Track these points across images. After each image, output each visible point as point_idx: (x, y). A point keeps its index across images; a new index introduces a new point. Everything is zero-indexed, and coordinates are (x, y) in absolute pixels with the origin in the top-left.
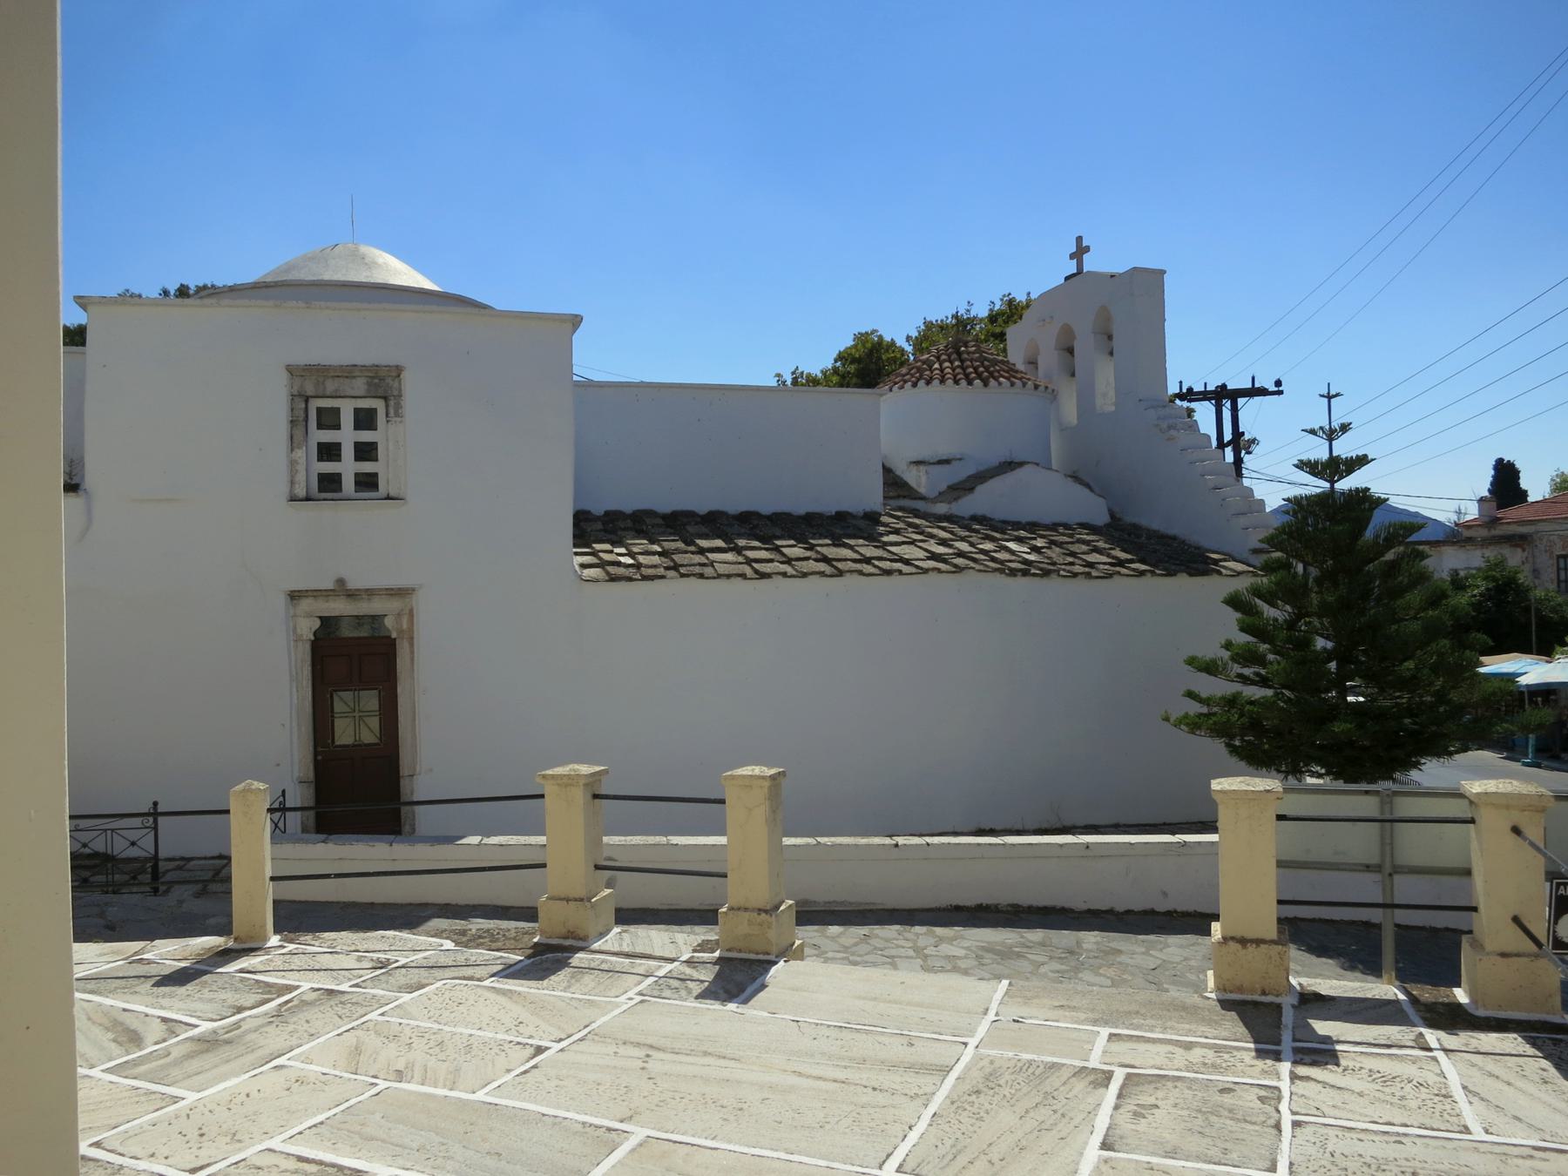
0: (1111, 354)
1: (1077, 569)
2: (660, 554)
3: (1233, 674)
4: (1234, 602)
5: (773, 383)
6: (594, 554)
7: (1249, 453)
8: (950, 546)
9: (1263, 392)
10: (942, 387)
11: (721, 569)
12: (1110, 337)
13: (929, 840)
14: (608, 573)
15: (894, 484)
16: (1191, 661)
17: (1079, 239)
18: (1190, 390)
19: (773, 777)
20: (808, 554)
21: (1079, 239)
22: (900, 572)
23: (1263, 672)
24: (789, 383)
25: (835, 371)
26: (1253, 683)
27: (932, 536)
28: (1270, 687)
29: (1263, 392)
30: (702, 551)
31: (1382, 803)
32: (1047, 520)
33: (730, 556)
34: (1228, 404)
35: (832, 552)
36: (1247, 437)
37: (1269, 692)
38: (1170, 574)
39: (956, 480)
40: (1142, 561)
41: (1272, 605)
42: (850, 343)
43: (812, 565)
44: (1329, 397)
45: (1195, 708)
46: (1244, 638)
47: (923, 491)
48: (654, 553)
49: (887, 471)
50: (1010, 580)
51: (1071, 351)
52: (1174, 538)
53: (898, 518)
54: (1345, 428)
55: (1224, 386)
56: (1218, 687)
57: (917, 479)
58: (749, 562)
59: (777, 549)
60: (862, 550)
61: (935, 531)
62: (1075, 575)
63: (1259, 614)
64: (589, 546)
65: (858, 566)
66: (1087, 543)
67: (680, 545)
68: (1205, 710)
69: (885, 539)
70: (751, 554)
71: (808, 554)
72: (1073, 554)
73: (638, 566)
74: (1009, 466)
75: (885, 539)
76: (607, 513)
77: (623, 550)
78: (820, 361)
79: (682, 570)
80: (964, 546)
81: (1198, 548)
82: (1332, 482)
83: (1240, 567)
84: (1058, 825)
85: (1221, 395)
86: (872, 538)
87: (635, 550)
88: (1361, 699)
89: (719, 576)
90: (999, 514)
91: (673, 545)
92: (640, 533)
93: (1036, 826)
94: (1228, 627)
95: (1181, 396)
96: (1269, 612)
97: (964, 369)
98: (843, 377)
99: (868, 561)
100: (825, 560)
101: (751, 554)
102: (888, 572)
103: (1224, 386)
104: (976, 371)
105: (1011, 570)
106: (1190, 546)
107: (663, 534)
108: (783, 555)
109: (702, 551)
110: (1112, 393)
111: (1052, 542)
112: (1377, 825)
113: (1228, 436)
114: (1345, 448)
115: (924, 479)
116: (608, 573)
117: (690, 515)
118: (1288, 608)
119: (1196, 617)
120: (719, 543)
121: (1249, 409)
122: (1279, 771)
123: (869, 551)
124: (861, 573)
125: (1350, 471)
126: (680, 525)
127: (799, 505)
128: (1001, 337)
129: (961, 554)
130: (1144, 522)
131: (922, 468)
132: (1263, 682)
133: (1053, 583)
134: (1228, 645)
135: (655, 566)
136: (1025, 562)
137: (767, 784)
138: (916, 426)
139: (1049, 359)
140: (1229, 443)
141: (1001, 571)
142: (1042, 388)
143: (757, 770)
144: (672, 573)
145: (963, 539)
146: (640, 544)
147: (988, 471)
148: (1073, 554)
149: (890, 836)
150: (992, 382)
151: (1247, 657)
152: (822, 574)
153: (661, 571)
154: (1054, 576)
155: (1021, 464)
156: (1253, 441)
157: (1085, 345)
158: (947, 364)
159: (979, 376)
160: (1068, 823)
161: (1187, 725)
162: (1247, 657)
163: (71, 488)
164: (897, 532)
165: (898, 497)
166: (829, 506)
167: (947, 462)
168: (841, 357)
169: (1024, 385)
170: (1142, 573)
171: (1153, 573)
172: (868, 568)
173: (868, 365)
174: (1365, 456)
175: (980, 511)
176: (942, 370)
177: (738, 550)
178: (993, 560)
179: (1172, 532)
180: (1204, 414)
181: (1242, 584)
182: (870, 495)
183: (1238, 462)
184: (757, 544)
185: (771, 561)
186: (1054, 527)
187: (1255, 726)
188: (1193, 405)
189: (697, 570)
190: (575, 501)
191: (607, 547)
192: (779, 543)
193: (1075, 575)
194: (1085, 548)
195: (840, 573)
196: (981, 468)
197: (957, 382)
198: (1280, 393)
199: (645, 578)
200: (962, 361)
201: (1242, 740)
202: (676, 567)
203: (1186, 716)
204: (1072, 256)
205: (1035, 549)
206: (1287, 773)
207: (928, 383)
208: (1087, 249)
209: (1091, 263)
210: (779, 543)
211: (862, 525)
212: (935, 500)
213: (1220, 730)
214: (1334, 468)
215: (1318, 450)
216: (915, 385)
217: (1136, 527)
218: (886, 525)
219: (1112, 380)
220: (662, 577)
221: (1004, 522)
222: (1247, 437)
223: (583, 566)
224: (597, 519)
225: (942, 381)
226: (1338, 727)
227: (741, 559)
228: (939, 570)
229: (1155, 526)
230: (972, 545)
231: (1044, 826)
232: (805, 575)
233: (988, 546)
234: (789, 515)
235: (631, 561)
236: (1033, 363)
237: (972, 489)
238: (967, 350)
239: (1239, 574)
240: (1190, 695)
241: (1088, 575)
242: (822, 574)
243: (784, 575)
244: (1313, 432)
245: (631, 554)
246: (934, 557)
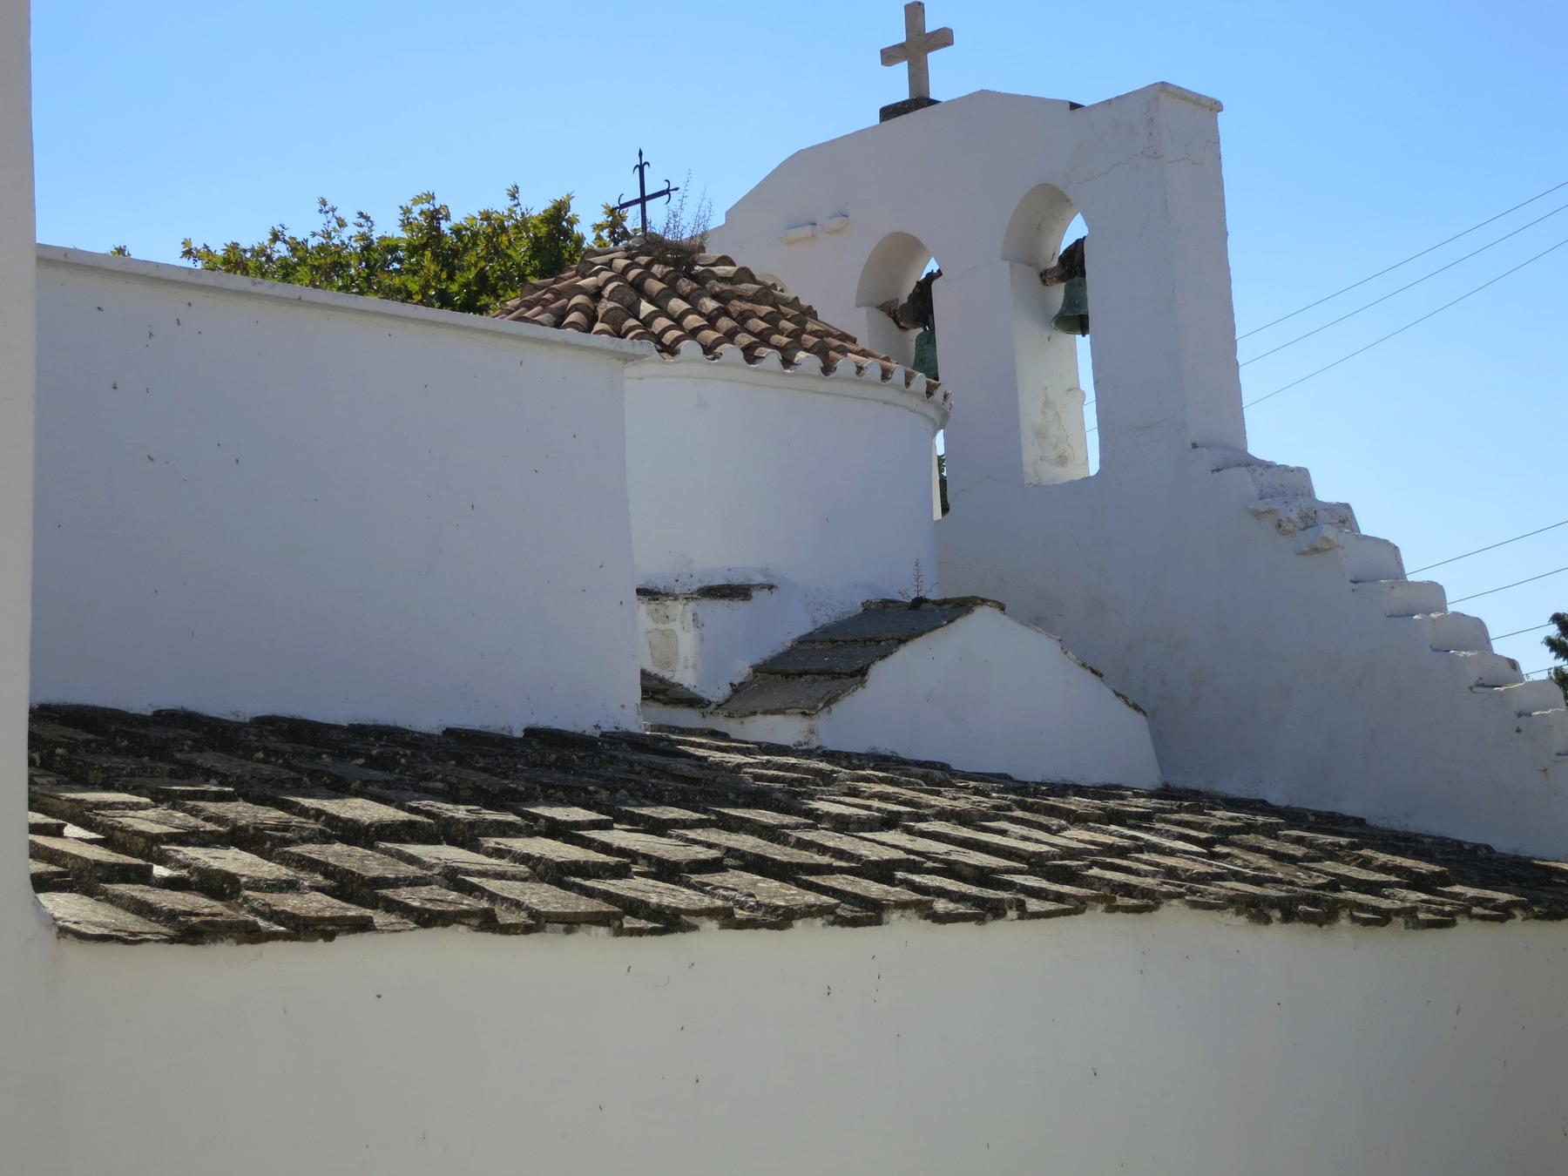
17: (914, 13)
126: (293, 755)
155: (961, 606)
163: (1194, 446)
166: (237, 697)
167: (735, 592)
185: (483, 874)
190: (33, 688)
193: (1383, 918)
196: (824, 618)
204: (889, 56)
209: (949, 77)
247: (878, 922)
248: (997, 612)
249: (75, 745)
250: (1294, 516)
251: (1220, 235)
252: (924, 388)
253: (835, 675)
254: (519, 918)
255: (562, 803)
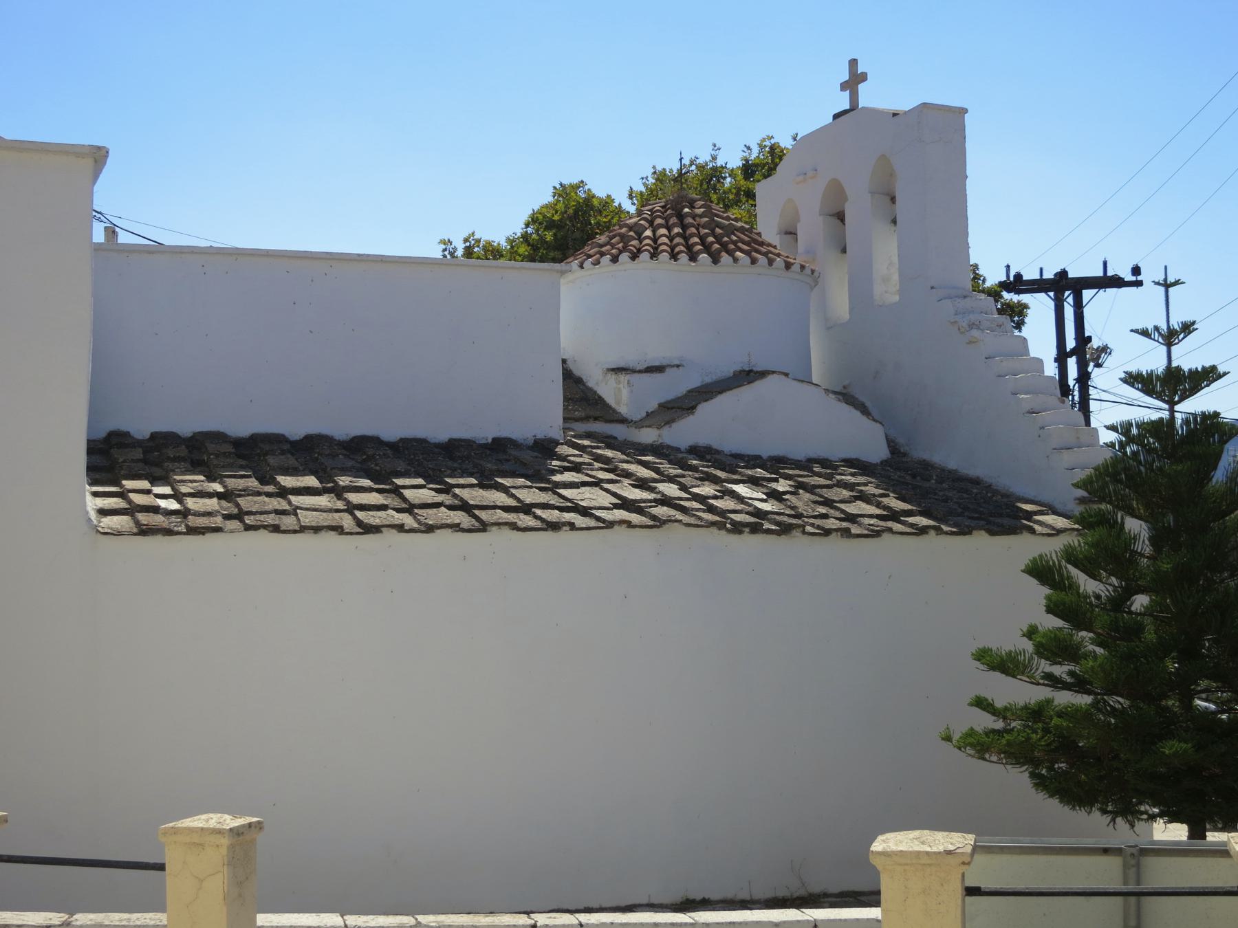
0: (894, 222)
1: (832, 523)
2: (220, 496)
3: (1038, 674)
4: (1040, 571)
5: (436, 252)
6: (122, 495)
7: (1098, 365)
8: (652, 490)
9: (1117, 282)
10: (653, 264)
11: (307, 518)
12: (893, 200)
13: (584, 918)
14: (137, 523)
15: (580, 397)
16: (982, 656)
17: (853, 63)
18: (1018, 276)
19: (236, 832)
20: (440, 498)
21: (853, 63)
22: (572, 526)
23: (1077, 669)
24: (460, 252)
25: (525, 237)
26: (1066, 686)
27: (627, 475)
28: (1089, 693)
29: (1117, 282)
30: (283, 493)
31: (1126, 867)
32: (799, 454)
33: (323, 501)
34: (1070, 300)
35: (474, 496)
36: (1095, 343)
37: (1084, 700)
38: (964, 531)
39: (670, 396)
40: (925, 513)
41: (1093, 576)
42: (548, 198)
43: (445, 516)
44: (1167, 285)
45: (985, 722)
46: (1055, 622)
47: (623, 410)
48: (210, 495)
49: (570, 378)
50: (734, 538)
51: (841, 217)
52: (976, 482)
53: (582, 448)
54: (1188, 328)
55: (1063, 273)
56: (1017, 693)
57: (618, 394)
58: (351, 508)
59: (396, 491)
60: (520, 494)
61: (633, 468)
62: (827, 532)
63: (1072, 587)
64: (116, 483)
65: (511, 517)
66: (846, 486)
67: (253, 483)
68: (1000, 725)
69: (557, 478)
70: (354, 498)
71: (440, 498)
72: (828, 503)
73: (184, 513)
74: (748, 376)
75: (557, 478)
76: (154, 436)
77: (167, 490)
78: (505, 223)
79: (249, 520)
80: (671, 490)
81: (1007, 495)
82: (1172, 404)
83: (1061, 522)
84: (802, 892)
85: (1063, 286)
86: (539, 476)
87: (184, 489)
88: (1213, 707)
89: (303, 529)
90: (730, 443)
91: (242, 483)
92: (196, 465)
93: (769, 894)
94: (1031, 605)
95: (1006, 286)
96: (1088, 585)
97: (686, 239)
98: (535, 248)
99: (527, 509)
100: (465, 507)
101: (354, 498)
102: (554, 526)
103: (1063, 273)
104: (703, 243)
105: (734, 523)
106: (996, 492)
107: (230, 466)
108: (404, 499)
109: (283, 493)
110: (896, 277)
111: (802, 486)
112: (1119, 899)
113: (1071, 343)
114: (1188, 356)
115: (625, 392)
116: (137, 523)
117: (275, 441)
118: (1114, 580)
119: (989, 590)
120: (311, 481)
121: (1097, 304)
122: (1104, 811)
123: (531, 496)
124: (513, 526)
125: (1194, 390)
126: (323, 457)
127: (343, 424)
128: (750, 195)
129: (665, 501)
130: (938, 458)
131: (623, 378)
132: (1079, 685)
133: (796, 544)
134: (1031, 633)
135: (209, 514)
136: (759, 513)
137: (225, 841)
138: (602, 316)
139: (812, 227)
140: (1073, 352)
141: (720, 526)
142: (796, 268)
143: (212, 820)
144: (234, 524)
145: (671, 479)
146: (192, 481)
147: (716, 383)
148: (828, 503)
149: (528, 913)
150: (725, 258)
151: (1055, 648)
152: (456, 527)
153: (218, 521)
154: (796, 533)
155: (763, 374)
156: (1104, 349)
157: (858, 208)
158: (663, 231)
159: (707, 248)
160: (816, 888)
161: (972, 745)
162: (1055, 648)
164: (577, 468)
165: (586, 419)
167: (659, 369)
168: (534, 220)
169: (771, 262)
170: (923, 531)
171: (938, 530)
172: (525, 520)
173: (569, 230)
174: (1214, 368)
175: (702, 440)
176: (655, 240)
177: (338, 492)
178: (712, 509)
179: (973, 472)
180: (1040, 307)
181: (1051, 548)
182: (542, 414)
183: (1084, 378)
184: (366, 483)
185: (383, 508)
186: (806, 465)
187: (1065, 746)
188: (1025, 298)
189: (271, 519)
191: (144, 484)
192: (399, 482)
193: (827, 532)
194: (846, 493)
195: (483, 527)
196: (708, 380)
197: (674, 256)
198: (1139, 284)
199: (192, 531)
200: (684, 227)
201: (1050, 769)
202: (239, 516)
203: (971, 733)
204: (844, 86)
205: (774, 495)
206: (1115, 814)
207: (634, 257)
208: (863, 77)
209: (868, 97)
210: (399, 482)
211: (524, 458)
212: (639, 424)
213: (1018, 753)
214: (1174, 384)
215: (1153, 359)
216: (615, 260)
217: (926, 465)
218: (563, 458)
219: (895, 259)
220: (218, 530)
221: (738, 456)
222: (1095, 343)
223: (103, 512)
224: (137, 443)
225: (654, 255)
226: (1170, 747)
227: (340, 505)
228: (629, 524)
229: (952, 465)
230: (683, 488)
231: (781, 894)
232: (430, 529)
233: (707, 490)
234: (422, 442)
235: (173, 505)
236: (790, 233)
237: (691, 409)
238: (699, 213)
239: (1059, 532)
240: (981, 703)
241: (846, 533)
242: (456, 527)
243: (400, 528)
244: (1145, 333)
245: (177, 496)
246: (626, 504)
247: (484, 530)
248: (783, 377)
249: (111, 458)
250: (964, 324)
251: (961, 176)
252: (783, 265)
253: (683, 409)
254: (1045, 530)
255: (462, 477)
